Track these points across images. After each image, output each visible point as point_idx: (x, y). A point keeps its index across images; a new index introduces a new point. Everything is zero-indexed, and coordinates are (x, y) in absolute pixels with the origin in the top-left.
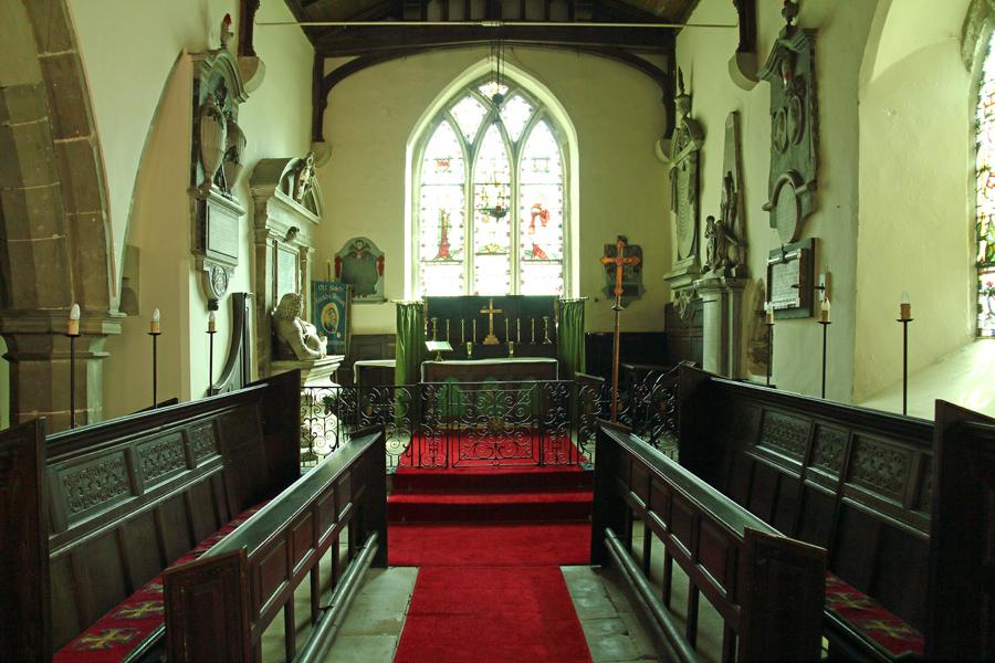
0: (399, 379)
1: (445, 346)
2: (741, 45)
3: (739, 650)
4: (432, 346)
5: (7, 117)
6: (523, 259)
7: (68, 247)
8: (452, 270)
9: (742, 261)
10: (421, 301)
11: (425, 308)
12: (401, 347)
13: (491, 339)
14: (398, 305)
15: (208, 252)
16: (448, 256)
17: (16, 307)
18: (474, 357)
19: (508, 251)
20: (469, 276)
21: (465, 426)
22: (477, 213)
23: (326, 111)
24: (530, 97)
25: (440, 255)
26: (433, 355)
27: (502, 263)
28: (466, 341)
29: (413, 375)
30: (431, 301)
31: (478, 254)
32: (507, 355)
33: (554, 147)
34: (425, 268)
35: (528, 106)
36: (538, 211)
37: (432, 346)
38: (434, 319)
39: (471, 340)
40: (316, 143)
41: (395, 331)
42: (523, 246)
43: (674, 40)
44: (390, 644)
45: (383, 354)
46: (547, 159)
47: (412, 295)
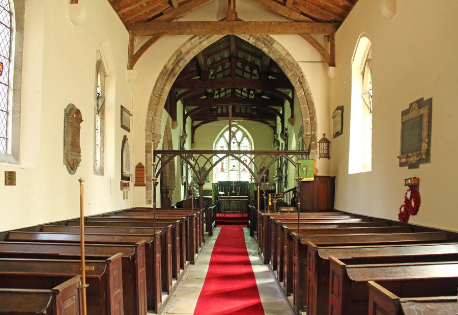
0: (213, 200)
1: (223, 193)
4: (220, 193)
12: (213, 193)
13: (233, 192)
29: (216, 198)
37: (220, 193)
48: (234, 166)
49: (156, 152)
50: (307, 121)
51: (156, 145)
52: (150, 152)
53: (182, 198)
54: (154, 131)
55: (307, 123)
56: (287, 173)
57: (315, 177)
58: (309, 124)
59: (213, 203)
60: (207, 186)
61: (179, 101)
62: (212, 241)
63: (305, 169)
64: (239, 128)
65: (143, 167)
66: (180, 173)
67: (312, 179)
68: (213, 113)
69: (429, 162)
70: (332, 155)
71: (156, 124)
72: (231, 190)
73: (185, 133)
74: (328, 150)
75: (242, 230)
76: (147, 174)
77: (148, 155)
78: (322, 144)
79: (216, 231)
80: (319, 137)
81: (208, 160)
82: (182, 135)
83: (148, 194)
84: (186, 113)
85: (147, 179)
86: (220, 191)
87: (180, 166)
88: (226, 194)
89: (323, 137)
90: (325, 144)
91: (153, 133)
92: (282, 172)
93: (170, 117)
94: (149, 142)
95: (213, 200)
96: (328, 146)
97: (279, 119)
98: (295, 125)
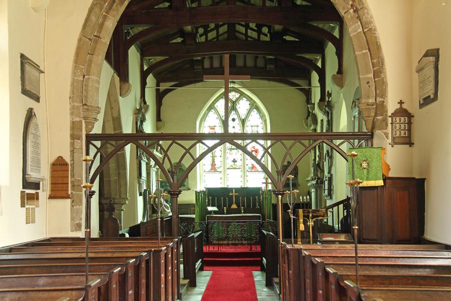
0: (197, 221)
1: (215, 209)
2: (321, 98)
3: (111, 55)
4: (210, 208)
5: (107, 148)
6: (248, 171)
7: (117, 180)
8: (216, 176)
9: (322, 178)
10: (204, 189)
11: (206, 193)
12: (197, 209)
13: (234, 206)
14: (196, 192)
15: (142, 178)
16: (215, 169)
17: (105, 197)
18: (227, 213)
19: (241, 167)
20: (224, 178)
21: (225, 242)
22: (227, 150)
23: (162, 107)
24: (249, 99)
25: (212, 169)
26: (211, 212)
27: (238, 173)
28: (224, 206)
29: (202, 218)
30: (209, 190)
31: (228, 169)
32: (241, 213)
33: (260, 121)
34: (206, 175)
35: (248, 102)
36: (254, 149)
37: (210, 208)
38: (210, 197)
39: (226, 206)
40: (159, 122)
41: (195, 202)
42: (247, 165)
43: (311, 75)
44: (200, 297)
45: (189, 212)
46: (258, 126)
47: (201, 187)
48: (234, 161)
49: (90, 138)
50: (368, 78)
51: (90, 124)
52: (79, 138)
53: (140, 219)
54: (86, 100)
55: (368, 83)
56: (333, 172)
57: (385, 179)
58: (372, 84)
59: (197, 227)
60: (187, 197)
63: (365, 165)
65: (67, 164)
66: (136, 174)
67: (380, 183)
70: (416, 139)
71: (90, 88)
73: (145, 103)
74: (409, 130)
76: (73, 176)
77: (76, 144)
78: (398, 119)
80: (392, 106)
81: (187, 151)
83: (74, 214)
85: (73, 186)
87: (135, 161)
89: (398, 106)
90: (402, 119)
91: (85, 105)
92: (323, 171)
93: (116, 75)
94: (78, 119)
95: (197, 221)
96: (410, 123)
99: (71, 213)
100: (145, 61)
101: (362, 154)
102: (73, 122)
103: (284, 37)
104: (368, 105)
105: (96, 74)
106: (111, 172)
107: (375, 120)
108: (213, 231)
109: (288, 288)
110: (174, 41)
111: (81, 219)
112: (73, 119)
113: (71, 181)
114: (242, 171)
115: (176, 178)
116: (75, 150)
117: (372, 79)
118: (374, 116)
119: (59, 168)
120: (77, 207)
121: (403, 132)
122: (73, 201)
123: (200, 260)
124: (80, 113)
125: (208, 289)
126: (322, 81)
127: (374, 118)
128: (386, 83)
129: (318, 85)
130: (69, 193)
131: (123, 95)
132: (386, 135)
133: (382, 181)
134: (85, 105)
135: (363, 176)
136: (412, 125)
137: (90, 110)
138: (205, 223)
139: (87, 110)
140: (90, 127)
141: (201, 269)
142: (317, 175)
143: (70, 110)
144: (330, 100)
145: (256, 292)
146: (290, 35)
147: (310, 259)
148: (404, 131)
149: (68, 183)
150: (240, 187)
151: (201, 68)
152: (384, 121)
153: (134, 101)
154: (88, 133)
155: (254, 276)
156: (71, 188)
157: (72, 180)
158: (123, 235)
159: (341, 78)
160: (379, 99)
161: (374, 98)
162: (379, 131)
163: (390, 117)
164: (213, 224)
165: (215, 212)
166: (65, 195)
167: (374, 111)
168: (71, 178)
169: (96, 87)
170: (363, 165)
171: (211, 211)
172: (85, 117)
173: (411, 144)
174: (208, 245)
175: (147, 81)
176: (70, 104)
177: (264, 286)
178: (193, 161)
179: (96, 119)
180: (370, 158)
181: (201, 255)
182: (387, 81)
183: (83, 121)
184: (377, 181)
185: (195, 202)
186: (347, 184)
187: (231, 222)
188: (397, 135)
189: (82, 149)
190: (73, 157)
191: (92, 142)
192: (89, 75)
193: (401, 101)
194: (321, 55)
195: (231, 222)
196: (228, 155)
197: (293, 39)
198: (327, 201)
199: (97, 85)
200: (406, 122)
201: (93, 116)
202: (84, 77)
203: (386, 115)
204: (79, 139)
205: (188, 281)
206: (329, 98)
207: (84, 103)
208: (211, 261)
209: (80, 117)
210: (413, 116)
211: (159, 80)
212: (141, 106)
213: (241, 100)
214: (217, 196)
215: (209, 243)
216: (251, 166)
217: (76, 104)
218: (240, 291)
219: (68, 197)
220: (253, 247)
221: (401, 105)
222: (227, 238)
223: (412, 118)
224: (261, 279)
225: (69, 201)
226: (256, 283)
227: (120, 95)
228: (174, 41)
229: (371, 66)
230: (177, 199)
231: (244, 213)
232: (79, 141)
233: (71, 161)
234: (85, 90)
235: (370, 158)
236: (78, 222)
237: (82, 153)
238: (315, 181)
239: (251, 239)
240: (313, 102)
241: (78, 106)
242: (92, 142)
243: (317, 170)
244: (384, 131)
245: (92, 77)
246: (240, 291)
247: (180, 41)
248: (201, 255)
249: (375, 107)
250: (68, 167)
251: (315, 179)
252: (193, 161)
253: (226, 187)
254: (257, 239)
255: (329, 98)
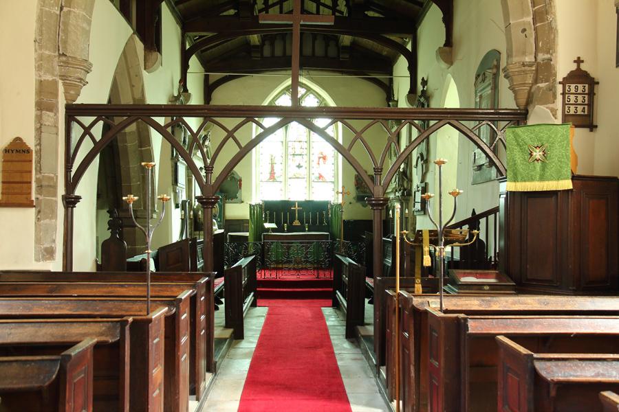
0: (251, 240)
1: (273, 226)
4: (267, 225)
12: (251, 226)
13: (296, 223)
14: (250, 205)
18: (288, 231)
19: (305, 177)
25: (270, 178)
26: (268, 230)
27: (303, 183)
28: (284, 223)
29: (257, 237)
32: (304, 231)
35: (316, 100)
37: (267, 225)
41: (248, 218)
45: (241, 229)
48: (299, 166)
49: (73, 111)
50: (524, 23)
51: (74, 86)
52: (52, 108)
53: (175, 237)
54: (65, 48)
55: (524, 30)
56: (427, 180)
57: (574, 178)
58: (531, 33)
59: (252, 250)
60: (236, 211)
61: (194, 56)
62: (239, 365)
63: (537, 154)
64: (309, 89)
65: (28, 151)
66: (170, 179)
67: (567, 184)
68: (253, 55)
69: (54, 259)
70: (601, 117)
71: (71, 28)
72: (292, 220)
73: (186, 90)
74: (591, 105)
75: (321, 317)
76: (39, 170)
77: (45, 118)
78: (573, 86)
79: (254, 321)
80: (563, 67)
81: (231, 134)
82: (176, 95)
83: (41, 233)
84: (188, 47)
85: (40, 187)
86: (266, 222)
87: (169, 164)
88: (280, 229)
89: (574, 67)
90: (580, 86)
91: (63, 55)
92: (410, 180)
93: (137, 39)
94: (49, 78)
95: (251, 240)
96: (591, 94)
97: (402, 64)
98: (455, 64)
99: (35, 231)
100: (188, 38)
101: (532, 135)
102: (41, 81)
103: (366, 13)
104: (524, 65)
105: (83, 7)
106: (132, 174)
107: (533, 90)
108: (270, 253)
109: (413, 381)
110: (225, 14)
111: (54, 241)
112: (40, 76)
113: (36, 178)
114: (306, 181)
115: (224, 187)
116: (43, 129)
117: (530, 24)
118: (532, 84)
119: (15, 156)
120: (47, 221)
121: (580, 108)
122: (39, 212)
123: (252, 294)
124: (53, 68)
125: (260, 345)
126: (413, 68)
127: (531, 87)
128: (556, 29)
129: (408, 74)
130: (33, 198)
131: (149, 68)
132: (554, 112)
133: (570, 181)
134: (63, 55)
135: (533, 173)
136: (595, 97)
137: (71, 64)
138: (260, 243)
139: (67, 63)
140: (72, 92)
141: (254, 305)
142: (403, 185)
143: (36, 63)
144: (425, 89)
145: (333, 353)
146: (374, 10)
147: (529, 364)
148: (582, 107)
149: (30, 183)
150: (304, 200)
151: (260, 56)
152: (551, 90)
153: (170, 85)
154: (70, 102)
155: (326, 317)
156: (36, 190)
157: (38, 176)
158: (143, 265)
159: (451, 52)
160: (541, 56)
161: (534, 55)
162: (542, 107)
163: (560, 83)
164: (270, 245)
165: (273, 230)
166: (25, 202)
167: (532, 75)
168: (36, 174)
169: (83, 29)
170: (534, 154)
171: (269, 229)
172: (63, 76)
173: (592, 127)
174: (264, 269)
175: (190, 64)
176: (36, 51)
177: (343, 338)
178: (239, 150)
179: (81, 79)
180: (548, 141)
181: (253, 285)
182: (556, 26)
183: (60, 83)
184: (561, 182)
185: (248, 218)
186: (450, 193)
187: (292, 243)
188: (571, 113)
189: (56, 127)
190: (40, 139)
191: (76, 117)
192: (70, 7)
193: (579, 58)
194: (411, 36)
195: (292, 243)
196: (290, 162)
197: (377, 15)
198: (418, 217)
199: (85, 25)
200: (587, 92)
201: (76, 75)
202: (61, 9)
203: (554, 80)
204: (51, 111)
205: (230, 331)
206: (424, 87)
207: (61, 52)
208: (268, 292)
209: (53, 75)
210: (598, 83)
211: (208, 65)
212: (179, 93)
213: (308, 97)
214: (278, 211)
215: (264, 267)
216: (318, 176)
217: (47, 52)
218: (309, 348)
219: (30, 205)
220: (321, 272)
221: (579, 66)
222: (289, 262)
223: (596, 86)
224: (336, 323)
225: (32, 211)
226: (331, 332)
227: (145, 69)
228: (225, 14)
229: (530, 4)
230: (212, 211)
231: (309, 231)
232: (52, 114)
233: (36, 146)
234: (63, 31)
235: (548, 141)
236: (48, 246)
237: (57, 134)
238: (400, 192)
239: (318, 262)
240: (396, 99)
241: (50, 56)
242: (76, 117)
243: (403, 180)
244: (551, 106)
245: (76, 10)
246: (309, 348)
247: (231, 14)
248: (253, 285)
249: (534, 68)
250: (32, 155)
251: (400, 190)
252: (239, 150)
253: (287, 199)
254: (325, 264)
255: (424, 87)
